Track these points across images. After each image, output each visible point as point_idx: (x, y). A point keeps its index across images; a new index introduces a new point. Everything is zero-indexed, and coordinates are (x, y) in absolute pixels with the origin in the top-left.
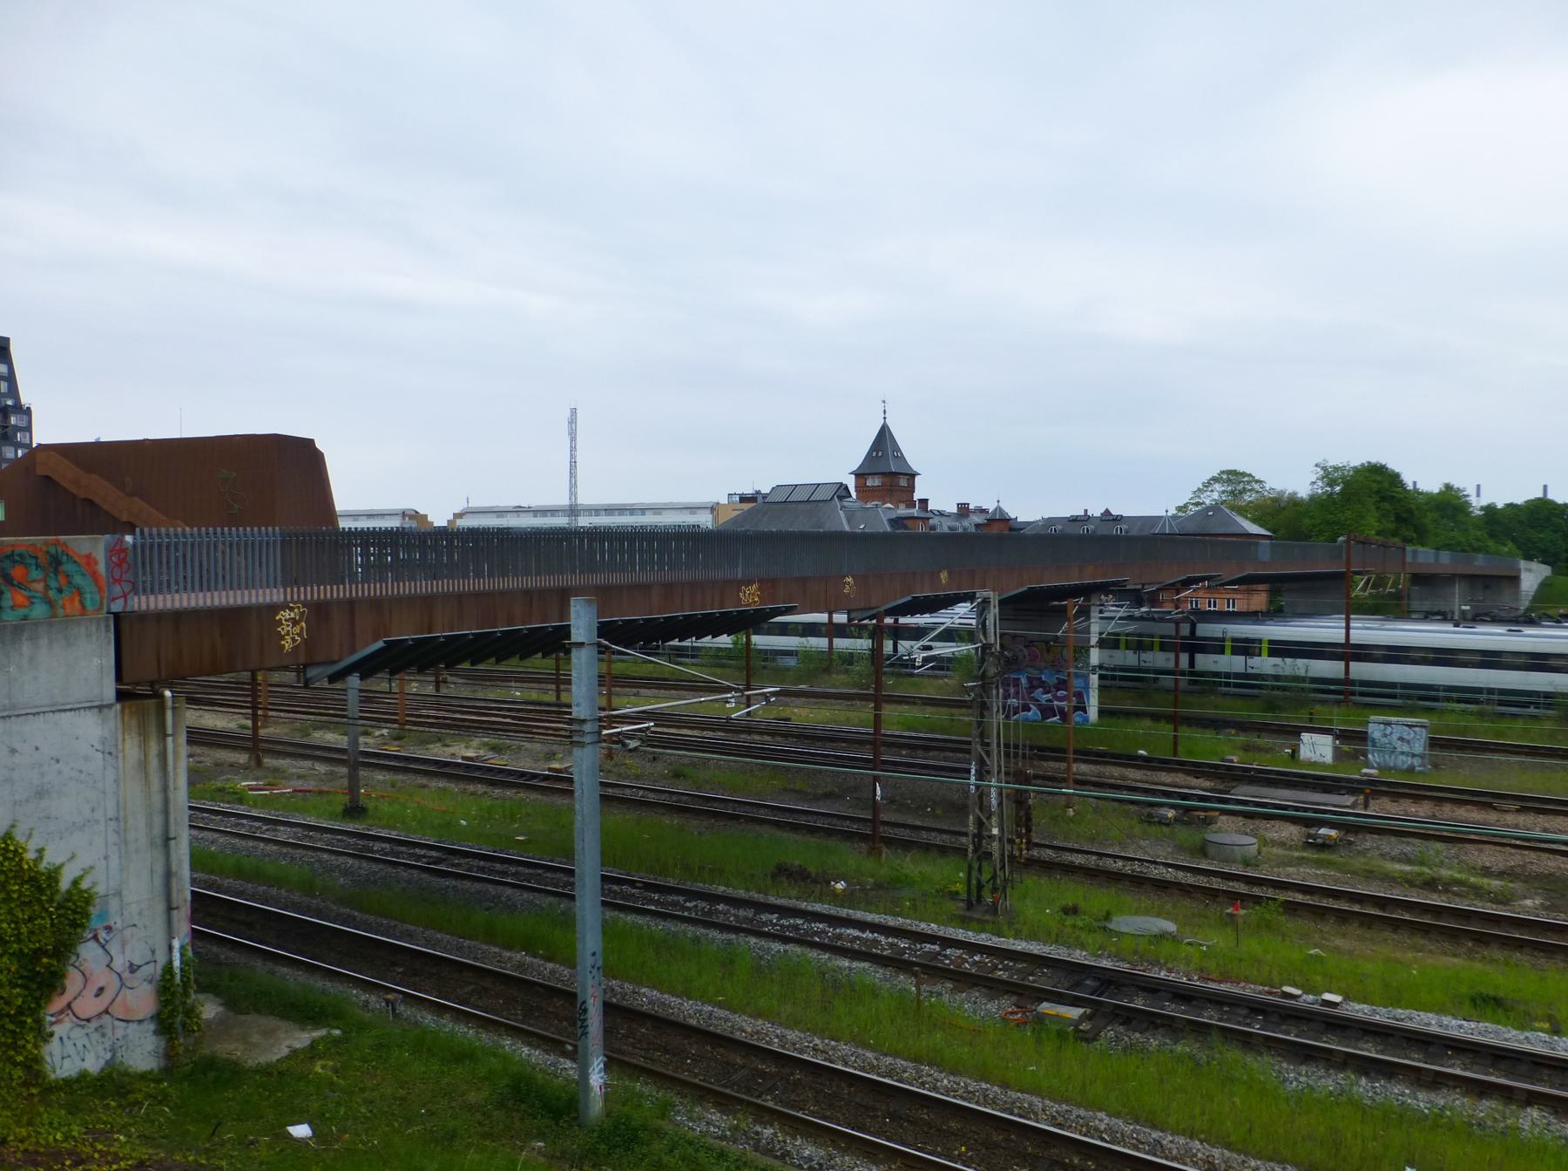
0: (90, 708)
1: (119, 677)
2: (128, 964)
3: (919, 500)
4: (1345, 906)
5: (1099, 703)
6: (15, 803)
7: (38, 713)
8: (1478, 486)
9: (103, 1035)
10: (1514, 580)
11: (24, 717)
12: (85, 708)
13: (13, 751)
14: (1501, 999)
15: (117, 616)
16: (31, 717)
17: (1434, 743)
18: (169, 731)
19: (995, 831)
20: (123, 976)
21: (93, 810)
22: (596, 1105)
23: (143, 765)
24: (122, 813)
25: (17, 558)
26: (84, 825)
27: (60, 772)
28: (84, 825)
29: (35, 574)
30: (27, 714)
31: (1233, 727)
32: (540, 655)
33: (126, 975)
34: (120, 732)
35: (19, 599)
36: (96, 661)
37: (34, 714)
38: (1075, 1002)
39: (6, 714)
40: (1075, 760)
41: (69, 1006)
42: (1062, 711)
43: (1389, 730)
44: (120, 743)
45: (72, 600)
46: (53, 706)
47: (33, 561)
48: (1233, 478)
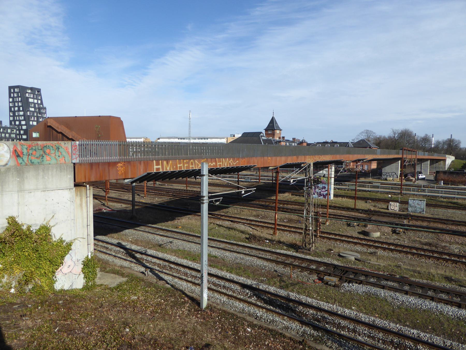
0: (67, 189)
1: (75, 181)
2: (77, 259)
3: (282, 137)
4: (263, 225)
5: (334, 193)
6: (47, 214)
7: (53, 190)
8: (433, 135)
9: (70, 278)
10: (445, 160)
11: (49, 191)
12: (66, 189)
13: (46, 200)
14: (244, 231)
15: (74, 164)
16: (51, 191)
17: (427, 205)
18: (88, 196)
19: (311, 228)
20: (75, 262)
21: (68, 217)
22: (205, 303)
23: (81, 205)
24: (75, 218)
25: (48, 147)
26: (65, 221)
27: (59, 206)
28: (65, 221)
29: (53, 152)
30: (50, 190)
31: (370, 200)
32: (175, 178)
33: (76, 262)
34: (75, 196)
35: (48, 159)
36: (69, 176)
37: (52, 190)
38: (335, 276)
39: (44, 190)
40: (329, 209)
41: (61, 270)
42: (323, 195)
43: (414, 201)
44: (75, 199)
45: (62, 159)
46: (57, 188)
47: (52, 148)
48: (367, 132)
